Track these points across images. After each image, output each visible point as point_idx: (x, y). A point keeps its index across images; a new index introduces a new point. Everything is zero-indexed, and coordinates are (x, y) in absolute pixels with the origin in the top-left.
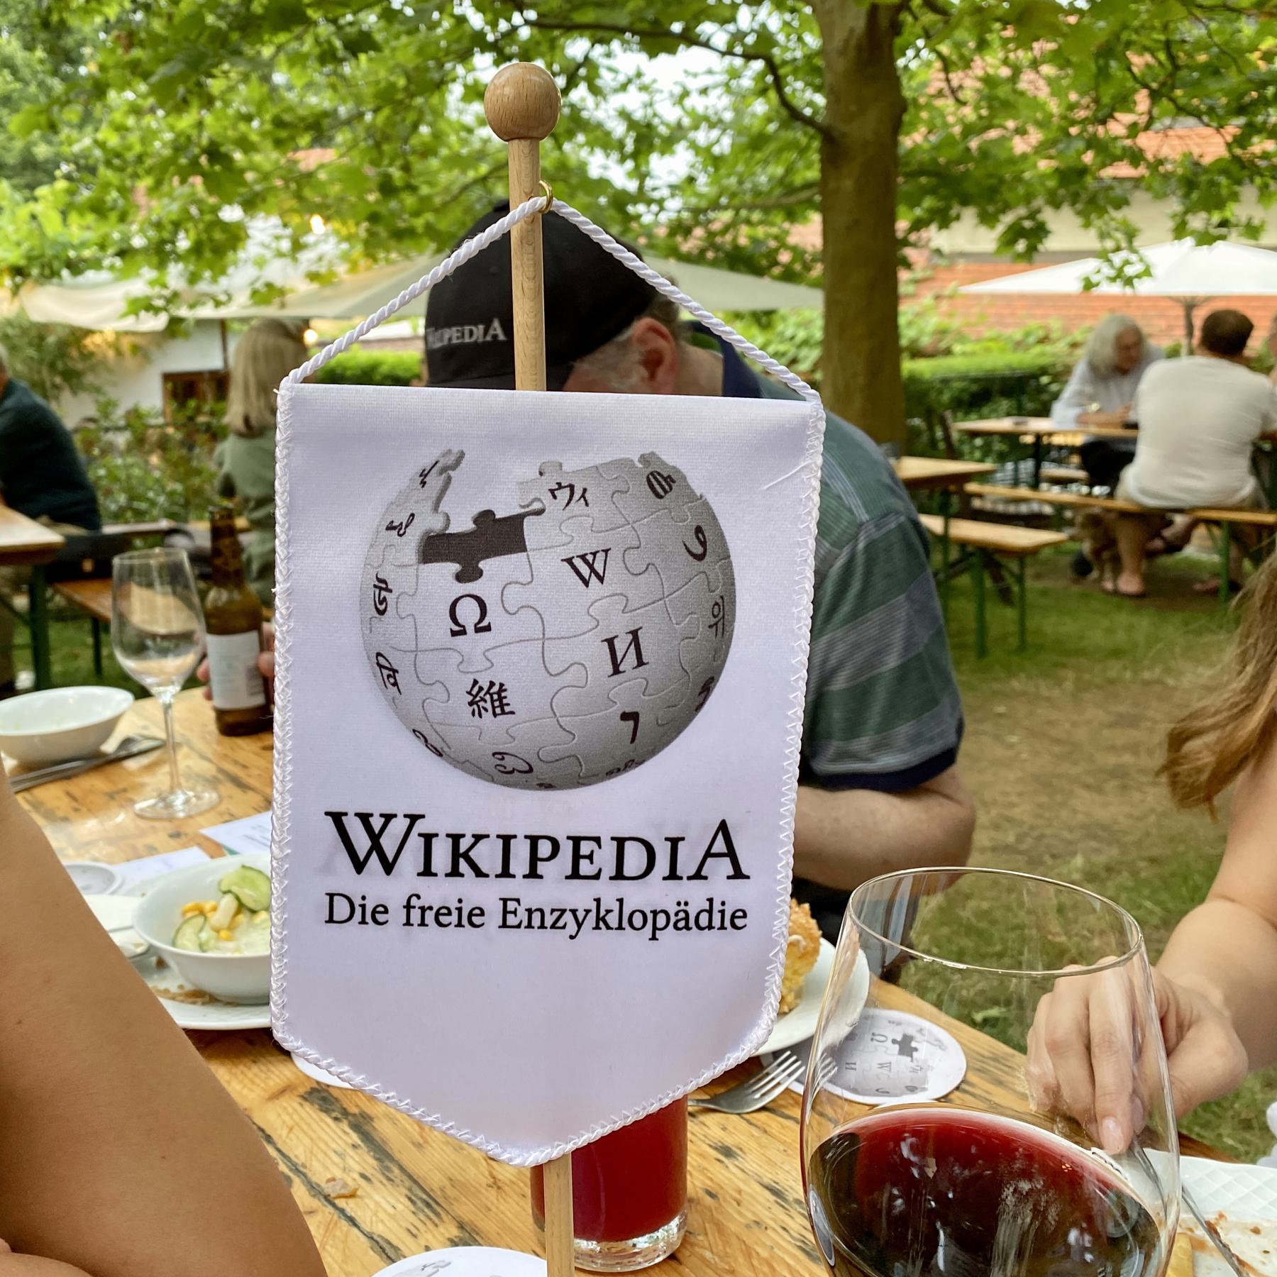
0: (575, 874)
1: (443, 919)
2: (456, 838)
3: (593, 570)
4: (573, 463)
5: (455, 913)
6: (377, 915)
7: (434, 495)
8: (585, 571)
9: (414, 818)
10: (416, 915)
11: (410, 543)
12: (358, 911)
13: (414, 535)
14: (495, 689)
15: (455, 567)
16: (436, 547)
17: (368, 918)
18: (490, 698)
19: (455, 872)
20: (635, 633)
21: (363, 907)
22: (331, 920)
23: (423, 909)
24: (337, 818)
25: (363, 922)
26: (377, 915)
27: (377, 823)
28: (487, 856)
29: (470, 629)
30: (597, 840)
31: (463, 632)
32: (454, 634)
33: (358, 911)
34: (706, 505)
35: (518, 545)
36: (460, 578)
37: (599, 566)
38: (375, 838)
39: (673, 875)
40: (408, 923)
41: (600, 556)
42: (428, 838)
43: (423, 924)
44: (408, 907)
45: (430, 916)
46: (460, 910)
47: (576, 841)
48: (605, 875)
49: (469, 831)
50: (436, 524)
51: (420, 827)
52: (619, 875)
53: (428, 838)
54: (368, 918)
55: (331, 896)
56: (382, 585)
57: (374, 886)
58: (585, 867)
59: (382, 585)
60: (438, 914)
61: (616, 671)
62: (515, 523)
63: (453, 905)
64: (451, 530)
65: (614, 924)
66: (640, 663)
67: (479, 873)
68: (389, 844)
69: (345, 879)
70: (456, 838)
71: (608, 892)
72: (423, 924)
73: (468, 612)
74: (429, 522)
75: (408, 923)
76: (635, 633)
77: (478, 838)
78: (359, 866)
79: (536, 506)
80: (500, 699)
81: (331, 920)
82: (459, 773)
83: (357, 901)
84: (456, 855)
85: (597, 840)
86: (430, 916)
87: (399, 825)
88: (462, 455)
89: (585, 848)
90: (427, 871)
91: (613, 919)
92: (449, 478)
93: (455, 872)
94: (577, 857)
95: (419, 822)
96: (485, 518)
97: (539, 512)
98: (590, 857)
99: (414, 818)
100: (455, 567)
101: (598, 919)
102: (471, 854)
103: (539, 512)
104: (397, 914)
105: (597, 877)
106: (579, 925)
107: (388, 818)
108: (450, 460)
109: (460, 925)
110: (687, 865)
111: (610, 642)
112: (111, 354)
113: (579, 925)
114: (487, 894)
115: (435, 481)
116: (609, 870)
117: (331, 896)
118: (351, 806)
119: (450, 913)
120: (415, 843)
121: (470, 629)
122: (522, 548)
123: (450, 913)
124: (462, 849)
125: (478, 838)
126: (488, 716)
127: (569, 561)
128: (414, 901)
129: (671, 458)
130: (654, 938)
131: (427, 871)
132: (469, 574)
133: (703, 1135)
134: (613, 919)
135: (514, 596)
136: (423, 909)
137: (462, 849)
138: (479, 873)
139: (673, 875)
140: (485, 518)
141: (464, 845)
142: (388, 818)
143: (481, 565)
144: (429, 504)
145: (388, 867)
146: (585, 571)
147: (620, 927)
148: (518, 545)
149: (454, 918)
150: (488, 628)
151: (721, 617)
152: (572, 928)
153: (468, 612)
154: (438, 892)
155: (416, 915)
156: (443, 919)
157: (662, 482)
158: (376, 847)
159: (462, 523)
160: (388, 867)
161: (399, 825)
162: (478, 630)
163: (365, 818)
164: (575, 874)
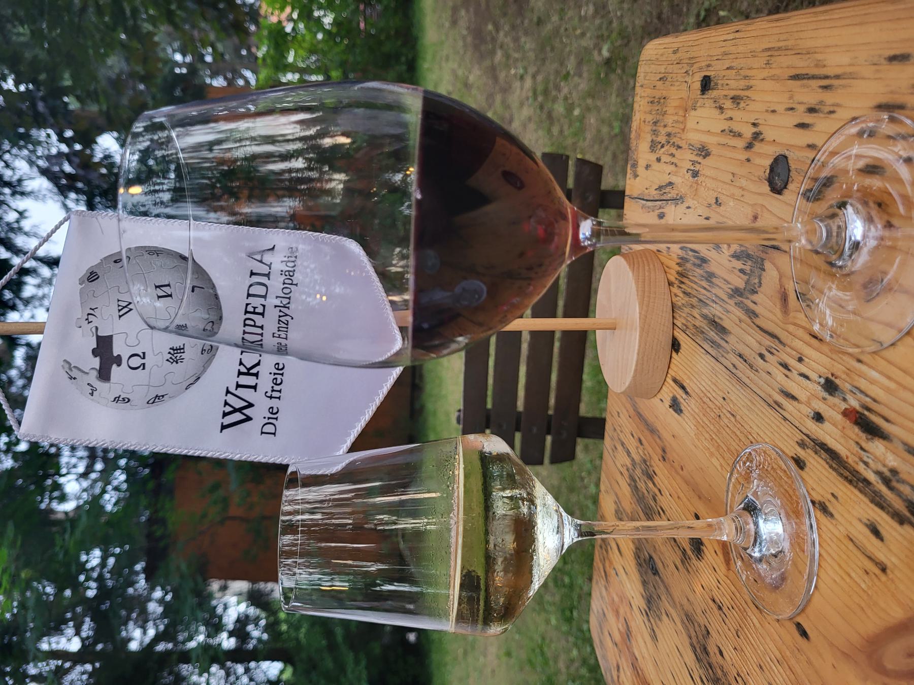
0: (262, 314)
1: (279, 382)
2: (240, 373)
3: (126, 307)
4: (79, 313)
5: (276, 376)
6: (274, 413)
7: (81, 374)
8: (126, 310)
9: (228, 392)
10: (275, 394)
11: (100, 385)
12: (271, 421)
13: (98, 384)
14: (172, 351)
15: (114, 367)
16: (104, 374)
17: (275, 416)
18: (176, 355)
19: (256, 375)
20: (156, 287)
21: (269, 418)
22: (274, 434)
23: (273, 391)
24: (224, 427)
25: (276, 419)
26: (274, 413)
27: (228, 409)
28: (250, 359)
29: (143, 361)
30: (247, 305)
31: (144, 364)
32: (144, 369)
33: (271, 421)
34: (105, 258)
35: (110, 339)
36: (119, 365)
37: (124, 304)
38: (235, 410)
39: (268, 275)
40: (279, 398)
41: (120, 303)
42: (238, 386)
43: (280, 391)
44: (271, 397)
45: (276, 388)
46: (275, 374)
47: (246, 312)
48: (264, 303)
49: (237, 367)
50: (95, 374)
51: (232, 390)
52: (265, 297)
53: (238, 386)
54: (275, 416)
55: (262, 433)
56: (117, 399)
57: (259, 413)
58: (260, 310)
59: (117, 399)
60: (276, 384)
61: (170, 296)
62: (99, 338)
63: (272, 377)
64: (98, 368)
65: (287, 301)
66: (169, 285)
67: (258, 364)
68: (239, 404)
69: (253, 427)
70: (240, 373)
71: (272, 301)
72: (280, 391)
73: (136, 362)
74: (93, 377)
75: (279, 398)
76: (156, 287)
77: (241, 363)
78: (249, 419)
79: (94, 330)
80: (177, 350)
81: (274, 434)
82: (208, 370)
83: (266, 421)
84: (248, 374)
85: (247, 305)
86: (276, 388)
87: (231, 399)
88: (65, 361)
89: (250, 309)
90: (254, 387)
91: (285, 301)
92: (75, 367)
93: (256, 375)
94: (254, 313)
95: (230, 390)
96: (95, 353)
97: (97, 328)
98: (255, 308)
99: (228, 392)
100: (114, 367)
101: (284, 307)
102: (248, 367)
103: (97, 328)
104: (274, 403)
105: (264, 306)
106: (287, 315)
107: (226, 404)
108: (67, 366)
109: (282, 374)
110: (265, 270)
111: (159, 297)
112: (358, 202)
113: (287, 315)
114: (268, 362)
115: (75, 373)
116: (262, 301)
117: (262, 433)
118: (219, 420)
119: (276, 379)
120: (241, 392)
121: (143, 361)
122: (111, 337)
123: (276, 379)
124: (246, 371)
125: (241, 363)
126: (184, 356)
127: (120, 316)
128: (269, 394)
129: (83, 271)
130: (296, 285)
131: (254, 387)
132: (118, 360)
133: (99, 334)
134: (285, 301)
135: (132, 340)
136: (273, 391)
137: (246, 371)
138: (258, 364)
139: (268, 275)
140: (95, 353)
141: (244, 370)
142: (226, 404)
143: (115, 354)
144: (85, 376)
145: (250, 405)
146: (126, 310)
147: (289, 298)
148: (110, 339)
149: (279, 377)
150: (144, 353)
151: (156, 252)
152: (288, 318)
153: (136, 362)
154: (265, 382)
155: (275, 394)
156: (279, 382)
157: (92, 276)
158: (240, 410)
159: (96, 362)
160: (250, 405)
161: (231, 399)
162: (144, 358)
163: (225, 414)
164: (262, 314)
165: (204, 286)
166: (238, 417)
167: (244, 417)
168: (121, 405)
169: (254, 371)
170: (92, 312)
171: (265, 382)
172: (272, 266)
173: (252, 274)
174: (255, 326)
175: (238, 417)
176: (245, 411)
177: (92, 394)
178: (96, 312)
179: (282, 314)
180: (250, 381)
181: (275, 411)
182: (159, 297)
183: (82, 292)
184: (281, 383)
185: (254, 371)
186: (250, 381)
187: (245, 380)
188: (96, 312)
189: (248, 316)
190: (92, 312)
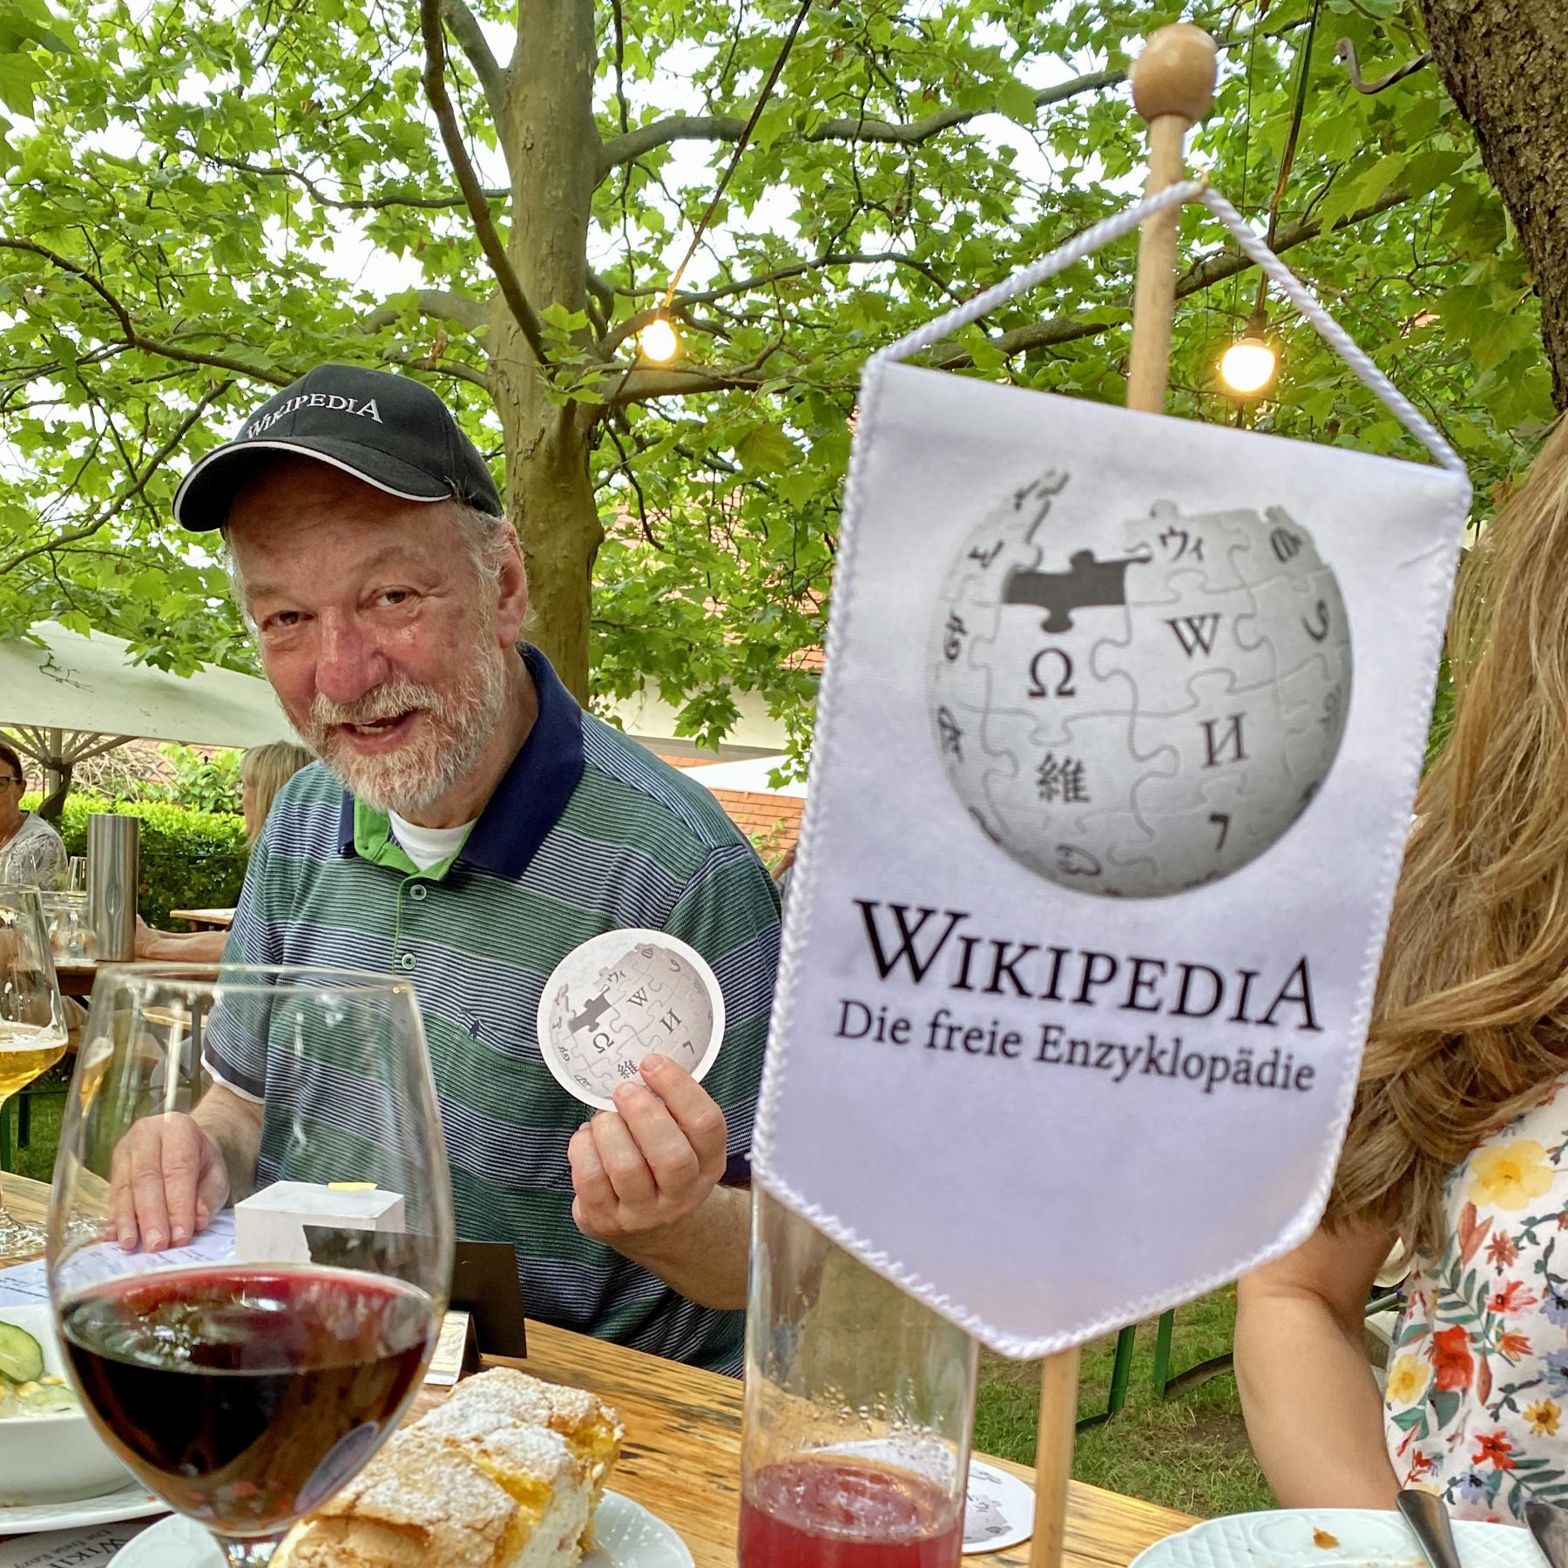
1: (974, 1044)
3: (1199, 639)
5: (987, 1038)
6: (897, 1031)
9: (956, 917)
12: (876, 1025)
14: (1071, 768)
15: (1042, 614)
16: (1024, 586)
17: (886, 1035)
19: (994, 988)
21: (882, 1020)
22: (842, 1033)
23: (951, 1030)
24: (867, 908)
25: (880, 1038)
26: (897, 1031)
27: (912, 918)
29: (1051, 691)
30: (1162, 964)
32: (1033, 694)
33: (876, 1025)
35: (1114, 595)
37: (1205, 634)
39: (1240, 1017)
40: (932, 1045)
42: (969, 943)
43: (949, 1047)
44: (935, 1025)
45: (958, 1038)
46: (993, 1034)
47: (1139, 963)
49: (1017, 938)
51: (963, 928)
53: (969, 943)
54: (886, 1035)
55: (847, 1003)
56: (956, 625)
57: (900, 996)
58: (1144, 997)
59: (956, 625)
60: (968, 1037)
61: (1211, 761)
62: (1118, 568)
63: (987, 1027)
67: (1022, 991)
68: (922, 946)
69: (866, 984)
70: (1001, 946)
71: (1165, 1027)
72: (949, 1047)
73: (1051, 671)
74: (1018, 555)
75: (932, 1045)
76: (1237, 720)
77: (1027, 948)
78: (884, 969)
79: (1142, 552)
80: (1076, 780)
81: (842, 1033)
83: (876, 1013)
84: (999, 967)
86: (958, 1038)
87: (938, 923)
88: (1065, 479)
89: (1147, 973)
90: (962, 984)
91: (1166, 1062)
93: (994, 988)
94: (1136, 983)
97: (1144, 560)
98: (1151, 985)
99: (956, 917)
100: (1042, 614)
102: (1018, 968)
103: (1144, 560)
104: (920, 1033)
105: (1155, 1009)
106: (1127, 1064)
108: (1051, 483)
109: (991, 1052)
110: (1255, 1009)
111: (1209, 727)
113: (1127, 1064)
114: (1024, 1017)
115: (1032, 505)
116: (1171, 1002)
117: (847, 1003)
118: (884, 897)
120: (954, 947)
121: (1051, 691)
123: (980, 1037)
125: (1027, 948)
126: (1058, 800)
127: (1173, 623)
128: (943, 1019)
130: (1208, 1090)
131: (962, 984)
134: (1166, 1062)
135: (1108, 658)
136: (951, 1030)
138: (1022, 991)
139: (1240, 1017)
140: (1083, 559)
142: (927, 913)
144: (1022, 533)
145: (918, 973)
148: (1114, 595)
149: (984, 1044)
150: (1071, 693)
151: (1334, 713)
152: (1118, 1068)
153: (1051, 671)
154: (971, 1009)
156: (974, 1044)
157: (1287, 543)
158: (908, 948)
160: (918, 973)
161: (938, 923)
164: (1131, 1004)
165: (1228, 843)
166: (891, 941)
167: (889, 957)
168: (943, 634)
169: (1005, 981)
170: (1191, 544)
171: (971, 1009)
172: (1265, 1029)
173: (1248, 976)
174: (1087, 981)
175: (891, 941)
176: (904, 961)
177: (974, 555)
178: (621, 979)
179: (1130, 1053)
180: (981, 972)
181: (900, 1035)
182: (1209, 727)
183: (1247, 515)
184: (968, 1049)
185: (1005, 981)
186: (981, 972)
187: (983, 960)
188: (621, 979)
189: (1126, 971)
190: (1191, 544)
